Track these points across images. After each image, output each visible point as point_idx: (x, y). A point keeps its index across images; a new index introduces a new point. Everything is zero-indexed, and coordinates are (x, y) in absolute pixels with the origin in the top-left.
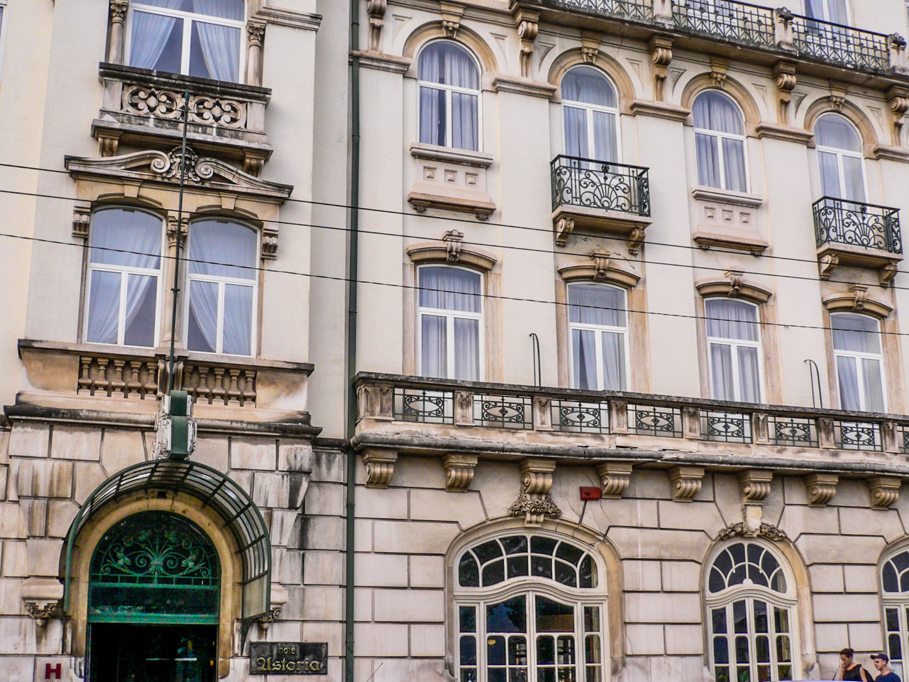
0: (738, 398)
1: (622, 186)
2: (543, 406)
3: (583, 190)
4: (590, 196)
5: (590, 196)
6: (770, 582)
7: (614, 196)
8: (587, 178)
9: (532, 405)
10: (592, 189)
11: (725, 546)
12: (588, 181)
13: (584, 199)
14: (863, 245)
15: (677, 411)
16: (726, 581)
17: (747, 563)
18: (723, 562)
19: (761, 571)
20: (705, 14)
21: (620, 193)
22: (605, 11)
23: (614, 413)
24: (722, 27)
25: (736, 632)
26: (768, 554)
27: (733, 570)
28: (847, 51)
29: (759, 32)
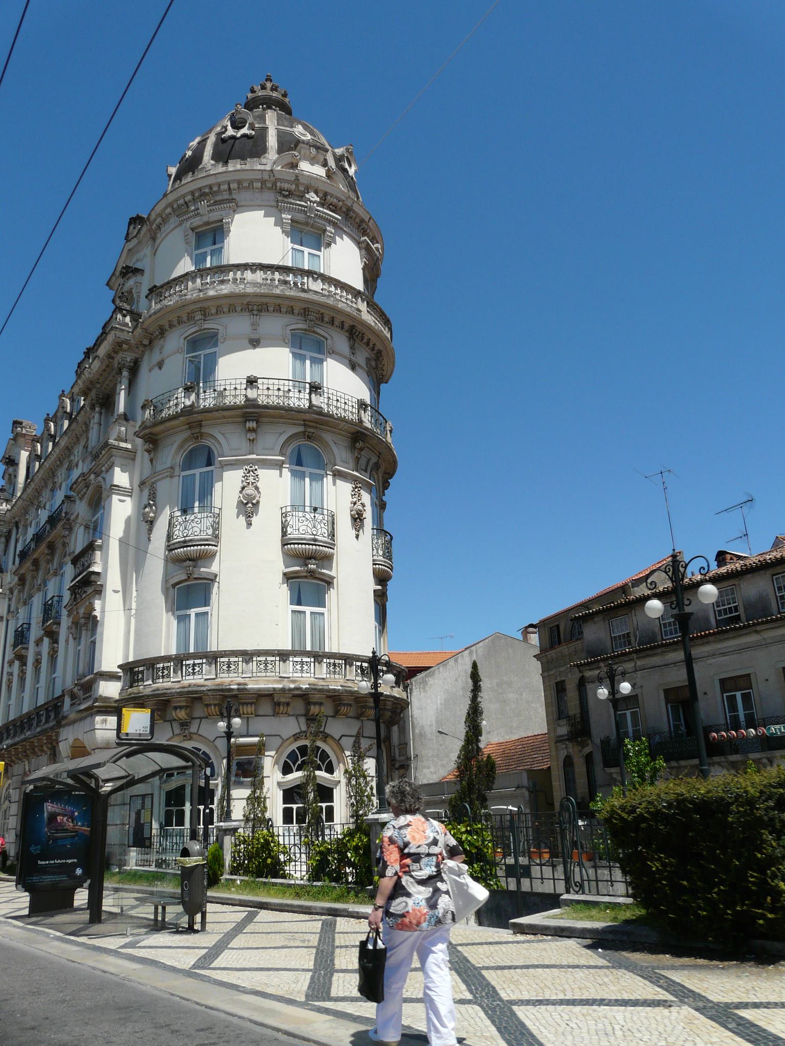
0: (308, 648)
2: (247, 662)
3: (300, 524)
4: (304, 528)
5: (304, 528)
6: (323, 769)
9: (314, 662)
10: (306, 523)
11: (294, 746)
12: (304, 519)
13: (301, 530)
14: (313, 535)
15: (278, 658)
16: (294, 769)
18: (292, 756)
19: (319, 762)
20: (347, 406)
22: (345, 417)
23: (316, 663)
24: (303, 401)
25: (284, 804)
26: (323, 751)
27: (299, 762)
28: (344, 409)
29: (336, 407)
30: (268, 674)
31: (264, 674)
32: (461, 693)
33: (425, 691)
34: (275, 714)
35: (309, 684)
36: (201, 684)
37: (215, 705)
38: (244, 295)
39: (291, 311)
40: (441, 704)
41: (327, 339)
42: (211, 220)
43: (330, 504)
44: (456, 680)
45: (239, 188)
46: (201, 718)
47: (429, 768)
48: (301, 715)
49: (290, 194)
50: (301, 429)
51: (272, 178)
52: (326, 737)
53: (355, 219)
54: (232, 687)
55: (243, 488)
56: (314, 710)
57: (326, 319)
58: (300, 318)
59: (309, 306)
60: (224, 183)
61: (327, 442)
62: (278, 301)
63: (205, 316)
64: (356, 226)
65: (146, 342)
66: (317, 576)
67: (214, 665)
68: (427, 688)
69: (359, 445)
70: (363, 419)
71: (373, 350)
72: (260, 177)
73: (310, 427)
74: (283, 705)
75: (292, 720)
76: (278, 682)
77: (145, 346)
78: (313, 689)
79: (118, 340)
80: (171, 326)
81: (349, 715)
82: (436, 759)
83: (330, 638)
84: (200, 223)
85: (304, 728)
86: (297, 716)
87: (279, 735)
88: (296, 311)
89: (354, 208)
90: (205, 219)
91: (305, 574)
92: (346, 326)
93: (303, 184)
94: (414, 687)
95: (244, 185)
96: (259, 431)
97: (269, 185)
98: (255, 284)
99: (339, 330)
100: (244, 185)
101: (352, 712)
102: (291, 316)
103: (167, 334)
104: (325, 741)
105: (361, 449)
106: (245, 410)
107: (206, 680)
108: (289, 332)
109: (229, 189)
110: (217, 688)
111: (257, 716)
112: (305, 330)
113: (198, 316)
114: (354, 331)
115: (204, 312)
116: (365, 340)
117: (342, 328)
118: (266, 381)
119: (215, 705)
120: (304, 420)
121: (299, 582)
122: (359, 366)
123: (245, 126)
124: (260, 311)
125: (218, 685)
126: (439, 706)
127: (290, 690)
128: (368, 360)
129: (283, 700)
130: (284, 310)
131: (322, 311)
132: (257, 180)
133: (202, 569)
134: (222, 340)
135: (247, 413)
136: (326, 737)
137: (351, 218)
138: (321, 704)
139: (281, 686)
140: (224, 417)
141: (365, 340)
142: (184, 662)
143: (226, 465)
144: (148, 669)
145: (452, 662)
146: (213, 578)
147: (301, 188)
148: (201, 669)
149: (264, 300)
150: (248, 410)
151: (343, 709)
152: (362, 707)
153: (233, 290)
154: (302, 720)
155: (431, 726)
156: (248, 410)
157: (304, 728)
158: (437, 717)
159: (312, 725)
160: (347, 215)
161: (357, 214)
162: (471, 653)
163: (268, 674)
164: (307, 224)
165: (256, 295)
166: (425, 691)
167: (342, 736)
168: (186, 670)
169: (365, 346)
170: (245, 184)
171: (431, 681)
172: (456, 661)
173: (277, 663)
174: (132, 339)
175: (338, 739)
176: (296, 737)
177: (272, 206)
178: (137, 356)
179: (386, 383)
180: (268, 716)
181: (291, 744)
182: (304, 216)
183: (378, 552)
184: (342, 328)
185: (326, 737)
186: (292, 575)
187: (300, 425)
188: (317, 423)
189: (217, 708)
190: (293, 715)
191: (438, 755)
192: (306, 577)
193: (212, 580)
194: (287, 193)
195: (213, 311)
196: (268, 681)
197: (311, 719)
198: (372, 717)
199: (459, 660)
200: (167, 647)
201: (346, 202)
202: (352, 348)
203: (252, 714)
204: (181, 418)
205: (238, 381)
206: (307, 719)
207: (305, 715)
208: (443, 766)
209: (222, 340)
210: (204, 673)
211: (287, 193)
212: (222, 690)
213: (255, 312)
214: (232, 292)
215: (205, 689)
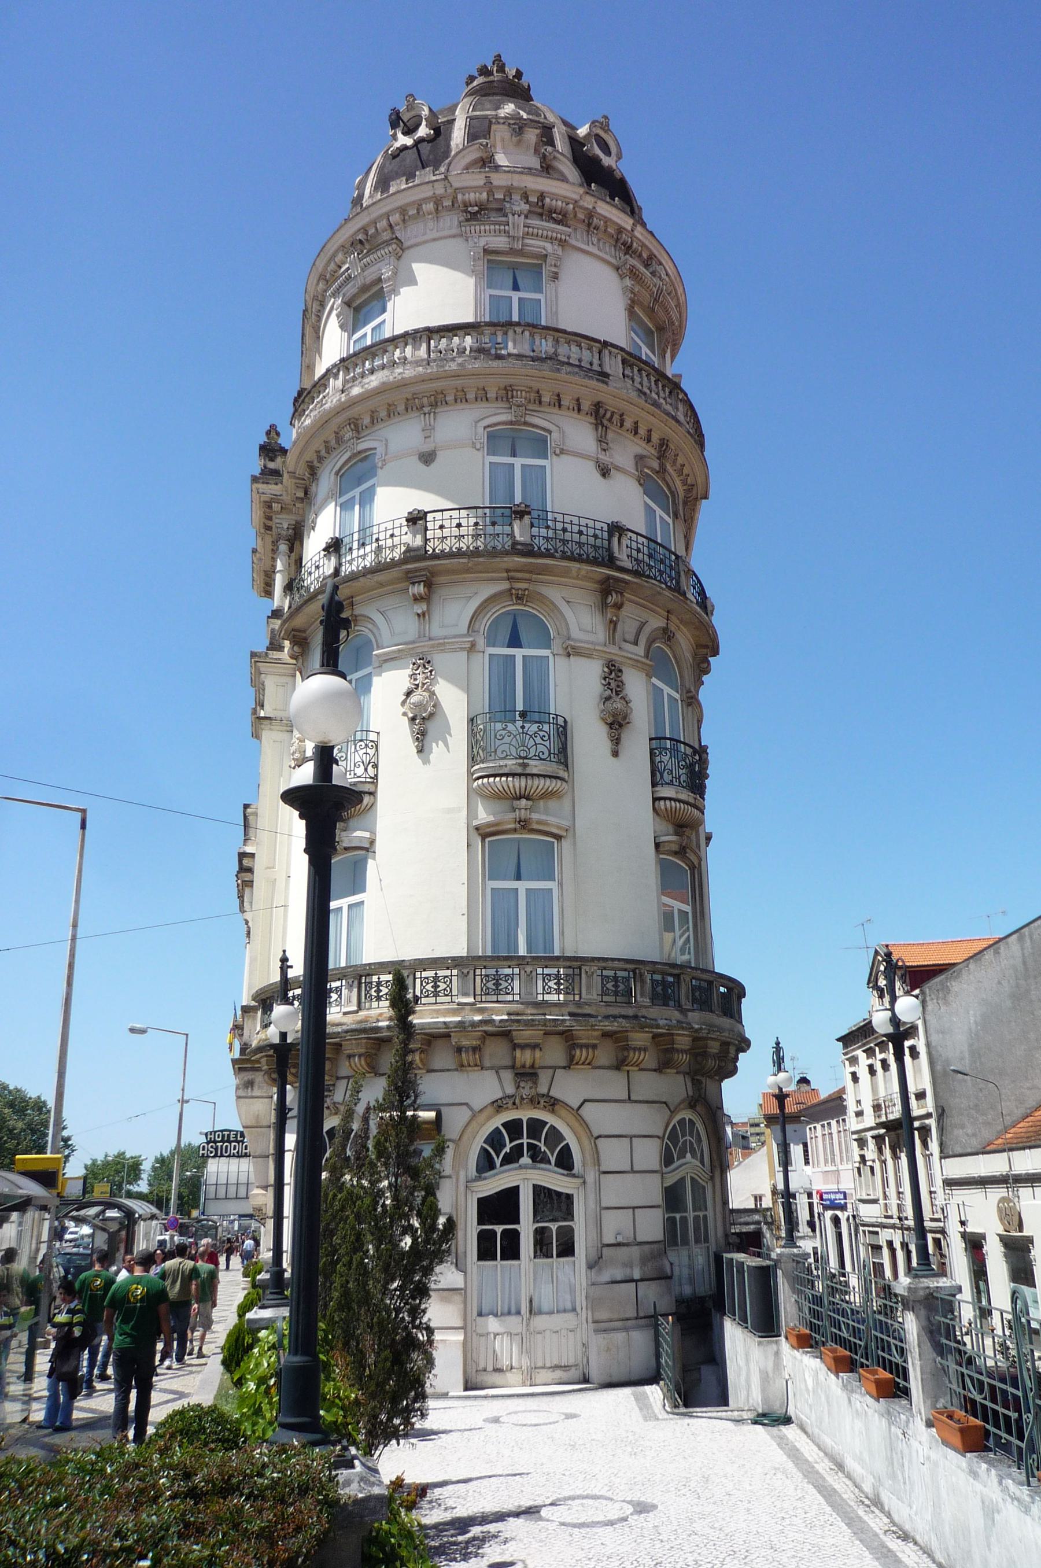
1: (542, 733)
3: (498, 742)
5: (506, 747)
7: (532, 743)
8: (504, 729)
10: (507, 739)
11: (498, 1121)
12: (503, 732)
14: (521, 758)
16: (498, 1162)
17: (525, 1141)
21: (538, 740)
27: (507, 1149)
29: (579, 543)
30: (440, 1000)
31: (494, 998)
32: (1009, 1003)
33: (947, 1003)
34: (461, 1067)
35: (509, 1014)
36: (337, 1021)
37: (360, 1056)
38: (402, 385)
39: (483, 396)
40: (976, 1022)
41: (550, 432)
42: (368, 280)
43: (558, 703)
44: (999, 983)
45: (404, 221)
46: (555, 1068)
47: (963, 1127)
48: (506, 1068)
49: (481, 209)
50: (505, 585)
51: (449, 191)
52: (553, 1104)
53: (605, 231)
54: (381, 1024)
55: (409, 694)
56: (525, 1057)
57: (546, 399)
58: (500, 405)
59: (512, 381)
60: (380, 218)
61: (553, 603)
62: (459, 382)
63: (358, 432)
64: (584, 227)
65: (301, 494)
66: (535, 826)
67: (355, 990)
68: (950, 998)
69: (612, 599)
70: (616, 554)
71: (649, 441)
72: (430, 194)
73: (519, 580)
74: (467, 1051)
75: (489, 1076)
76: (454, 1012)
77: (301, 500)
78: (513, 1021)
79: (264, 498)
80: (320, 459)
81: (642, 1066)
82: (973, 1112)
83: (562, 933)
84: (355, 290)
85: (510, 1090)
86: (497, 1070)
87: (466, 1104)
88: (491, 395)
89: (599, 210)
90: (359, 282)
91: (512, 826)
92: (586, 406)
93: (499, 187)
94: (928, 999)
95: (410, 213)
96: (435, 598)
97: (447, 203)
98: (418, 363)
99: (575, 415)
100: (410, 213)
101: (649, 1059)
102: (485, 404)
103: (319, 472)
104: (553, 1112)
105: (619, 606)
106: (405, 567)
107: (345, 1014)
108: (481, 430)
109: (391, 226)
110: (358, 1026)
111: (430, 1071)
112: (511, 423)
113: (348, 434)
114: (602, 411)
115: (356, 425)
116: (628, 424)
117: (579, 410)
118: (438, 515)
119: (360, 1056)
120: (507, 571)
121: (519, 840)
122: (618, 469)
123: (420, 125)
124: (434, 405)
125: (361, 1022)
126: (973, 1027)
127: (474, 1024)
128: (639, 459)
129: (465, 1043)
130: (471, 396)
131: (536, 385)
132: (425, 200)
133: (358, 833)
134: (380, 464)
135: (408, 572)
136: (553, 1104)
137: (596, 228)
138: (534, 1047)
139: (459, 1019)
140: (381, 585)
141: (628, 424)
142: (418, 975)
143: (386, 661)
144: (350, 987)
145: (989, 955)
146: (367, 845)
147: (499, 196)
148: (340, 996)
149: (437, 385)
150: (409, 566)
151: (634, 1057)
152: (666, 1051)
153: (385, 379)
154: (508, 1076)
155: (962, 1059)
156: (409, 566)
157: (510, 1090)
158: (971, 1045)
159: (522, 1084)
160: (589, 225)
161: (607, 220)
162: (1021, 939)
163: (440, 1000)
164: (512, 252)
165: (422, 380)
166: (947, 1003)
167: (585, 1101)
168: (367, 992)
169: (631, 436)
170: (412, 212)
171: (955, 986)
172: (997, 952)
173: (454, 979)
174: (284, 493)
175: (576, 1107)
176: (498, 1106)
177: (454, 236)
178: (299, 518)
179: (706, 497)
180: (448, 1070)
181: (489, 1118)
182: (506, 239)
183: (662, 777)
184: (579, 410)
185: (553, 1105)
186: (488, 830)
187: (503, 579)
188: (531, 572)
189: (362, 1058)
190: (491, 1068)
191: (976, 1105)
192: (515, 830)
193: (367, 850)
194: (476, 208)
195: (367, 420)
196: (437, 1011)
197: (526, 1074)
198: (685, 1068)
199: (1002, 950)
200: (484, 949)
201: (581, 203)
202: (602, 441)
203: (476, 1065)
204: (320, 597)
205: (397, 524)
206: (516, 1074)
207: (513, 1067)
208: (987, 1124)
209: (380, 464)
210: (455, 992)
211: (476, 208)
212: (364, 1031)
213: (426, 410)
214: (384, 383)
215: (339, 1029)
